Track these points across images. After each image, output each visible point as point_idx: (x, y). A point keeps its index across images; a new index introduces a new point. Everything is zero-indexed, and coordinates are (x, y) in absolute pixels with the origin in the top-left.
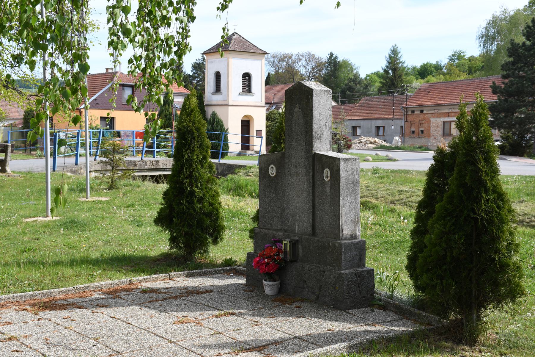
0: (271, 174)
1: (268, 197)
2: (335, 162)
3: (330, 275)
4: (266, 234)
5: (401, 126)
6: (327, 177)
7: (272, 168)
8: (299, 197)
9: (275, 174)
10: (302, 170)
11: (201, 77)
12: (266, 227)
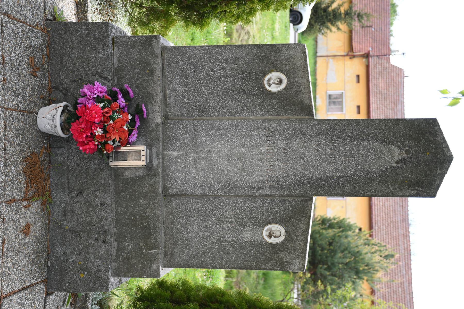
0: (269, 80)
1: (223, 69)
3: (101, 259)
4: (152, 73)
6: (270, 236)
7: (281, 82)
8: (230, 159)
9: (267, 86)
12: (166, 67)
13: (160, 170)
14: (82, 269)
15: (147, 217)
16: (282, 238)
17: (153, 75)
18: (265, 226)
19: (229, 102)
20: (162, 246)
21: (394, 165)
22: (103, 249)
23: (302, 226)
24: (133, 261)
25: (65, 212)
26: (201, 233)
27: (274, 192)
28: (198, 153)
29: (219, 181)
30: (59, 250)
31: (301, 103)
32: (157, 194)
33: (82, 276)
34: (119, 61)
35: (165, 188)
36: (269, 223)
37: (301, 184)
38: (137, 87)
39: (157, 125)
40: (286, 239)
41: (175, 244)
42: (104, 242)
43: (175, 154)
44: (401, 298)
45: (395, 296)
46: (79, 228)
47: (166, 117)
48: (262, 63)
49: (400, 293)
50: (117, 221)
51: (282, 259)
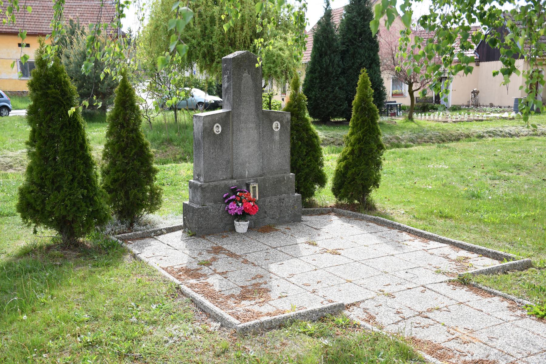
0: (217, 132)
2: (285, 116)
4: (216, 186)
5: (473, 92)
6: (278, 128)
7: (217, 126)
8: (249, 147)
9: (219, 133)
10: (252, 125)
11: (509, 67)
13: (255, 178)
14: (294, 207)
15: (273, 182)
16: (278, 122)
17: (217, 186)
18: (274, 130)
19: (225, 150)
20: (282, 175)
21: (250, 76)
22: (286, 199)
23: (273, 114)
24: (289, 187)
25: (273, 218)
26: (277, 158)
27: (261, 127)
28: (246, 162)
29: (257, 152)
30: (287, 218)
31: (225, 116)
32: (264, 179)
33: (296, 207)
34: (211, 202)
35: (261, 176)
36: (272, 128)
37: (258, 115)
38: (222, 192)
39: (237, 181)
40: (278, 121)
41: (281, 169)
42: (283, 199)
43: (247, 172)
44: (86, 10)
45: (85, 15)
46: (279, 211)
47: (232, 178)
48: (210, 135)
49: (81, 9)
50: (275, 195)
51: (286, 122)
